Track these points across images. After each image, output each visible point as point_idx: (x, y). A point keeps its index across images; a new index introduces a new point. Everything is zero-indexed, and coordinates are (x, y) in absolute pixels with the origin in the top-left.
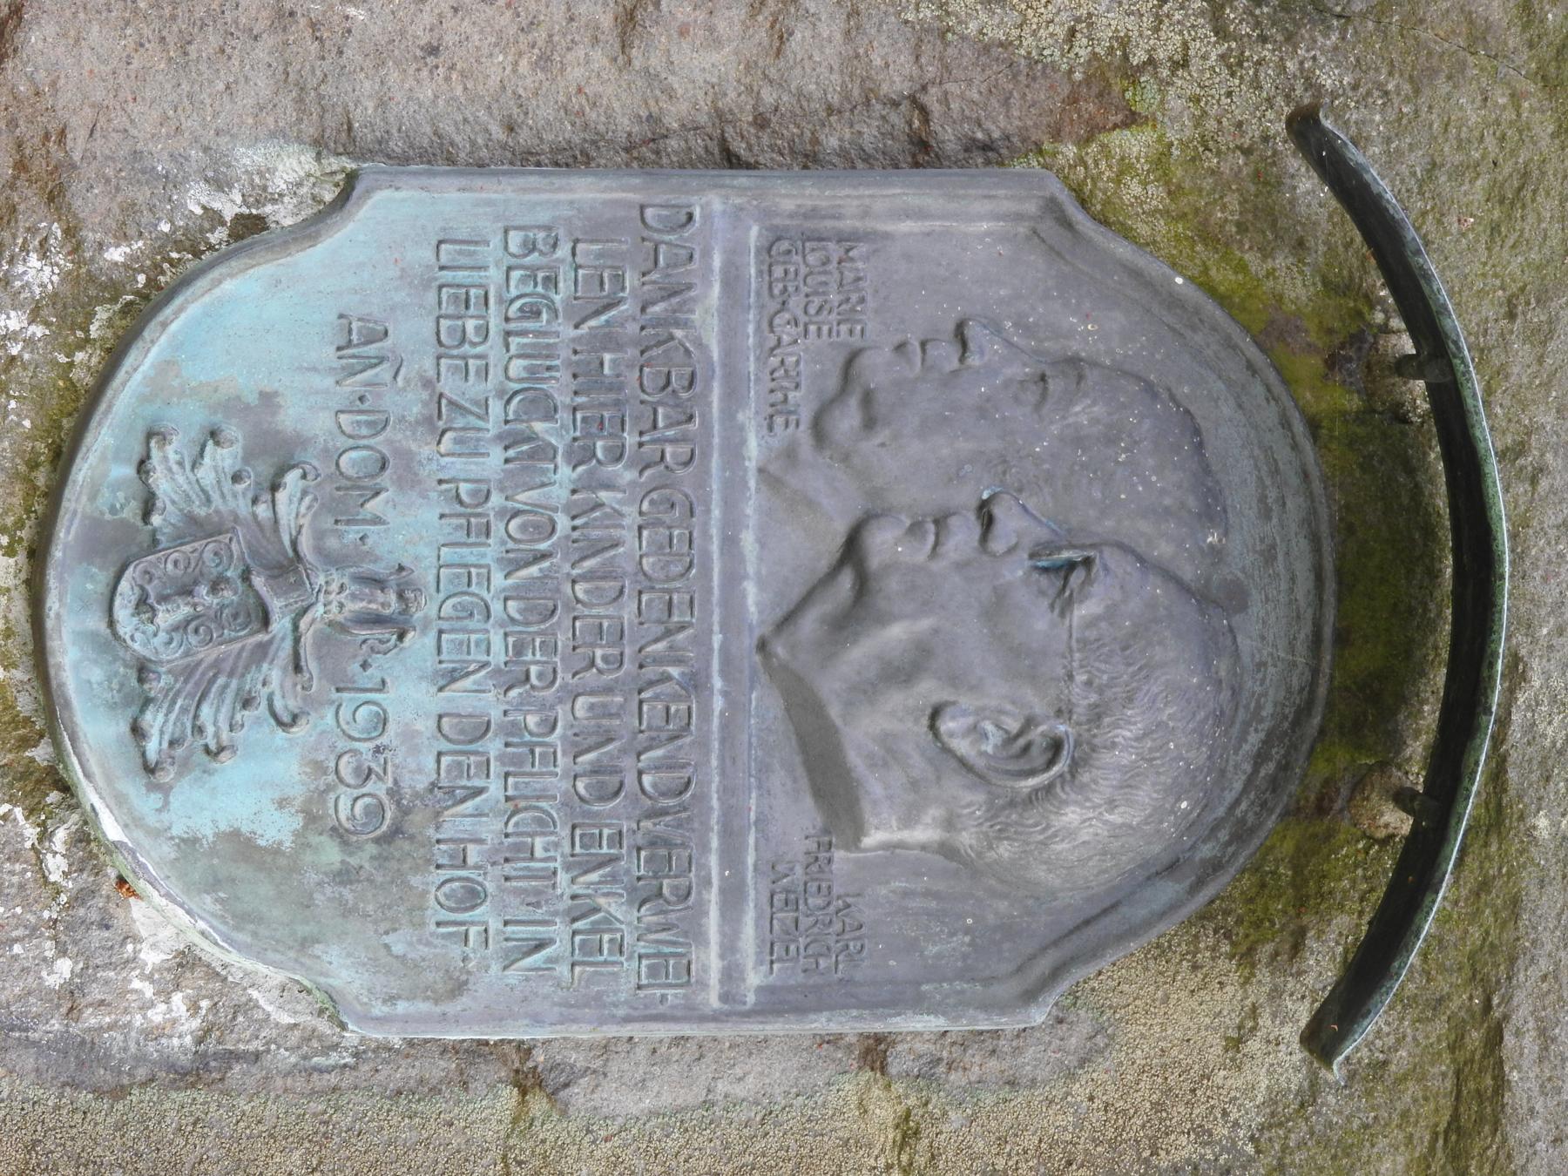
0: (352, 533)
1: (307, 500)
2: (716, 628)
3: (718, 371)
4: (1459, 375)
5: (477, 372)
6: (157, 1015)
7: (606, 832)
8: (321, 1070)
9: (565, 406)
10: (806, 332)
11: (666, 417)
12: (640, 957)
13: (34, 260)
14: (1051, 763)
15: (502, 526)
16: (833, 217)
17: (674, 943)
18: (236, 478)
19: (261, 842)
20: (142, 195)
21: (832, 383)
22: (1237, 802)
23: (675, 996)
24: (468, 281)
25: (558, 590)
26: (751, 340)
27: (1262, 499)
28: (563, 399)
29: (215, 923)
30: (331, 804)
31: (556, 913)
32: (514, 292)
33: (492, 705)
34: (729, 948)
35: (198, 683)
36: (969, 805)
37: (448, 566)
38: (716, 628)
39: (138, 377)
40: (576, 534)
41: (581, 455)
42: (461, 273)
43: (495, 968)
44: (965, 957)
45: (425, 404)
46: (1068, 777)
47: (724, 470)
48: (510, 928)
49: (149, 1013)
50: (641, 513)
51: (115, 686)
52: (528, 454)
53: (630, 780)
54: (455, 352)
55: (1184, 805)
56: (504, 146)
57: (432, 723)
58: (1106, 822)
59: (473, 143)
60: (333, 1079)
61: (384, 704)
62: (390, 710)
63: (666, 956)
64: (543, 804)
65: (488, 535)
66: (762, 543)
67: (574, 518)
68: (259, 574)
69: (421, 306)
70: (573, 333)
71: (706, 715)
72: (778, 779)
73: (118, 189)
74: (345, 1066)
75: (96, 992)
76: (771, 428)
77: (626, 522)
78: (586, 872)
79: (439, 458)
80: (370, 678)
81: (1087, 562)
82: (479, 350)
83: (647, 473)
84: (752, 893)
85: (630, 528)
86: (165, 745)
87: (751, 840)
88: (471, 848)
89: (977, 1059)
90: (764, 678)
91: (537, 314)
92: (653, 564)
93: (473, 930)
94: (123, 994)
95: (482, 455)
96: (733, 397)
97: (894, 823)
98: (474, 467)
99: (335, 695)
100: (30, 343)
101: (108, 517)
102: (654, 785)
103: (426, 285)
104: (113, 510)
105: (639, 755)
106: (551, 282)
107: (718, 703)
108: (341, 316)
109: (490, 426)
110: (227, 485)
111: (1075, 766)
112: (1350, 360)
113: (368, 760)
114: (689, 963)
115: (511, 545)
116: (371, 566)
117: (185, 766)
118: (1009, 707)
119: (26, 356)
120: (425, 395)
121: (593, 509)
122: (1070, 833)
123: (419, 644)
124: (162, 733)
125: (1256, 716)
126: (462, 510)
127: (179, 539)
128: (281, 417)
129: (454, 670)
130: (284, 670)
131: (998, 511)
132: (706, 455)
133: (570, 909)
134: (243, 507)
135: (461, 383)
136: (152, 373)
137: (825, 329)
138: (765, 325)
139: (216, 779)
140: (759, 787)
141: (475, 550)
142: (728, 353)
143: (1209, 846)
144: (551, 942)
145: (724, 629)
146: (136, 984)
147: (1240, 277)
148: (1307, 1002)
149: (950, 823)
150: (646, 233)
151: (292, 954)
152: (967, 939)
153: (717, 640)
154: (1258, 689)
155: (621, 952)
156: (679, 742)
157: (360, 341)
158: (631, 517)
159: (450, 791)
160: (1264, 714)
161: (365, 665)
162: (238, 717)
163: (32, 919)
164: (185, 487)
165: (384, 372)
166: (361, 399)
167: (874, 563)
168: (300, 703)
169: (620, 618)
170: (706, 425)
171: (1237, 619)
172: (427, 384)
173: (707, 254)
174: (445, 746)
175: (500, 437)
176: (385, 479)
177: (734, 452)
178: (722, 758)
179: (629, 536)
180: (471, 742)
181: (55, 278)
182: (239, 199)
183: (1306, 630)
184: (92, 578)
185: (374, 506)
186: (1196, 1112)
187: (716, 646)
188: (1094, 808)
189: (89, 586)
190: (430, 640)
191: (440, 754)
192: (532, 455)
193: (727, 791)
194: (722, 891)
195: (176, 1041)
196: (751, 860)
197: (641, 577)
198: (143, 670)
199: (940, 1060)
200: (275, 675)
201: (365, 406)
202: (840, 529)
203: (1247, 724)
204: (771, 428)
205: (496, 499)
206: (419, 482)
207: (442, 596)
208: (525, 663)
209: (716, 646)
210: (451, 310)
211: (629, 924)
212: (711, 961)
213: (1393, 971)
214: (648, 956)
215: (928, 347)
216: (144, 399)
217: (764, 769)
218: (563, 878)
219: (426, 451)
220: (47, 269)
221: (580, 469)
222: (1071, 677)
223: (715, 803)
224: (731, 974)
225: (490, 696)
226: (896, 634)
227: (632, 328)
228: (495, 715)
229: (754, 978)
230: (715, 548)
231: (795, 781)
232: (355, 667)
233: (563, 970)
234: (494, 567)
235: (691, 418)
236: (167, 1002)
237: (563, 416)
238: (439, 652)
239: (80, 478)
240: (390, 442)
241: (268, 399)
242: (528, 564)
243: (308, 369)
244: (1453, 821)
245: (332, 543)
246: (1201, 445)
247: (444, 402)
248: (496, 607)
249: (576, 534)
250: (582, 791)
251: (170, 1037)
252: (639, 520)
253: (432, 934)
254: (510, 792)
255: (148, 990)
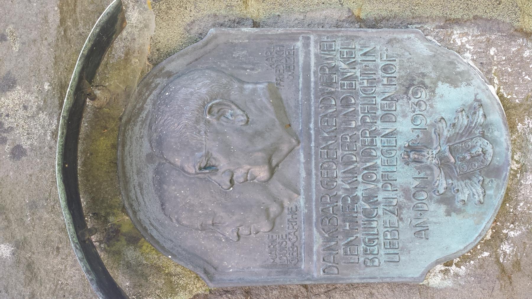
0: (422, 175)
1: (437, 184)
2: (313, 148)
3: (314, 225)
4: (75, 237)
5: (386, 223)
6: (465, 39)
7: (345, 88)
8: (418, 23)
9: (360, 213)
10: (286, 236)
11: (329, 210)
12: (335, 50)
13: (508, 252)
14: (211, 107)
15: (378, 177)
16: (279, 272)
17: (325, 54)
18: (458, 190)
19: (448, 85)
20: (479, 271)
21: (278, 221)
22: (149, 95)
23: (324, 39)
24: (390, 250)
25: (361, 159)
26: (303, 234)
27: (141, 189)
28: (361, 215)
29: (461, 61)
30: (428, 96)
31: (360, 64)
32: (376, 247)
33: (380, 125)
34: (307, 54)
35: (469, 130)
36: (236, 95)
37: (394, 165)
38: (313, 148)
39: (487, 220)
40: (356, 175)
41: (355, 199)
42: (392, 252)
43: (378, 47)
44: (234, 50)
45: (402, 213)
46: (206, 103)
47: (311, 195)
48: (374, 59)
49: (467, 40)
50: (336, 182)
51: (491, 130)
52: (370, 198)
53: (339, 103)
54: (393, 229)
55: (167, 94)
56: (373, 288)
57: (398, 119)
58: (193, 88)
59: (382, 289)
60: (414, 21)
61: (412, 125)
62: (411, 123)
63: (328, 50)
64: (364, 95)
65: (382, 175)
66: (298, 174)
67: (357, 180)
68: (452, 163)
69: (404, 242)
70: (358, 235)
71: (316, 123)
72: (292, 103)
73: (485, 273)
74: (410, 25)
75: (483, 45)
76: (296, 207)
77: (340, 179)
78: (352, 75)
79: (398, 198)
80: (416, 132)
81: (200, 169)
82: (386, 229)
83: (335, 194)
84: (300, 70)
85: (340, 177)
86: (477, 113)
87: (301, 85)
88: (385, 83)
89: (226, 23)
90: (297, 134)
91: (370, 240)
92: (332, 166)
93: (385, 59)
94: (475, 45)
95: (385, 198)
96: (308, 217)
97: (259, 90)
98: (387, 194)
99: (427, 127)
100: (508, 228)
101: (493, 179)
102: (331, 101)
103: (402, 249)
104: (492, 181)
105: (336, 111)
106: (366, 250)
107: (312, 126)
108: (427, 239)
109: (382, 207)
110: (460, 188)
111: (204, 106)
112: (112, 232)
113: (417, 108)
114: (320, 48)
115: (375, 172)
116: (417, 165)
117: (470, 107)
118: (225, 124)
119: (509, 224)
120: (402, 216)
121: (351, 183)
122: (204, 85)
123: (402, 142)
124: (479, 116)
125: (143, 122)
126: (390, 182)
127: (473, 174)
128: (444, 209)
129: (392, 135)
130: (442, 134)
131: (228, 183)
132: (317, 200)
133: (356, 65)
134: (455, 182)
135: (391, 219)
136: (482, 221)
137: (280, 238)
138: (299, 238)
139: (461, 103)
140: (298, 101)
141: (386, 170)
142: (311, 230)
143: (158, 82)
144: (361, 55)
145: (310, 148)
146: (472, 48)
147: (148, 256)
148: (124, 37)
149: (242, 89)
150: (337, 265)
151: (438, 52)
152: (234, 55)
153: (313, 144)
154: (142, 130)
155: (341, 52)
156: (324, 114)
157: (422, 232)
158: (339, 182)
159: (392, 100)
160: (140, 123)
161: (418, 136)
162: (456, 121)
163: (499, 66)
164: (472, 188)
165: (414, 222)
166: (421, 214)
167: (267, 167)
168: (437, 125)
169: (342, 150)
170: (317, 208)
171: (150, 151)
172: (401, 219)
173: (318, 260)
174: (393, 113)
175: (379, 204)
176: (413, 191)
177: (308, 200)
178: (310, 109)
179: (339, 174)
180: (387, 114)
181: (502, 246)
182: (451, 271)
183: (127, 148)
184: (497, 161)
185: (416, 183)
186: (158, 7)
187: (313, 143)
188: (197, 93)
189: (498, 159)
190: (399, 143)
191: (395, 110)
192: (370, 199)
193: (309, 100)
194: (310, 70)
195: (459, 32)
196: (301, 80)
197: (336, 163)
198: (483, 136)
199: (237, 23)
200: (446, 133)
201: (419, 212)
202: (274, 177)
203: (146, 119)
204: (296, 207)
205: (380, 185)
206: (403, 190)
207: (395, 157)
208: (370, 137)
209: (313, 143)
210: (395, 241)
211: (338, 60)
212: (313, 49)
213: (99, 28)
214: (332, 50)
215: (249, 233)
216: (484, 213)
217: (297, 107)
218: (358, 74)
219: (401, 199)
220: (504, 249)
221: (355, 195)
222: (205, 133)
223: (312, 96)
224: (307, 45)
225: (380, 127)
226: (260, 144)
227: (340, 237)
228: (379, 122)
229: (299, 44)
230: (314, 171)
231: (287, 103)
232: (421, 136)
233: (358, 47)
234: (380, 166)
235: (322, 211)
236: (462, 43)
237: (360, 210)
238: (396, 140)
239: (503, 190)
240: (412, 202)
241: (448, 214)
242: (370, 166)
243: (437, 223)
244: (77, 79)
245: (428, 172)
246: (162, 205)
247: (396, 214)
248: (379, 153)
249: (356, 175)
250: (353, 99)
251: (460, 33)
252: (337, 180)
253: (397, 58)
254: (374, 99)
255: (467, 46)
